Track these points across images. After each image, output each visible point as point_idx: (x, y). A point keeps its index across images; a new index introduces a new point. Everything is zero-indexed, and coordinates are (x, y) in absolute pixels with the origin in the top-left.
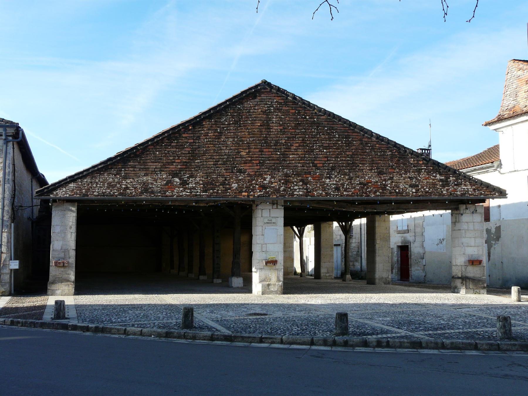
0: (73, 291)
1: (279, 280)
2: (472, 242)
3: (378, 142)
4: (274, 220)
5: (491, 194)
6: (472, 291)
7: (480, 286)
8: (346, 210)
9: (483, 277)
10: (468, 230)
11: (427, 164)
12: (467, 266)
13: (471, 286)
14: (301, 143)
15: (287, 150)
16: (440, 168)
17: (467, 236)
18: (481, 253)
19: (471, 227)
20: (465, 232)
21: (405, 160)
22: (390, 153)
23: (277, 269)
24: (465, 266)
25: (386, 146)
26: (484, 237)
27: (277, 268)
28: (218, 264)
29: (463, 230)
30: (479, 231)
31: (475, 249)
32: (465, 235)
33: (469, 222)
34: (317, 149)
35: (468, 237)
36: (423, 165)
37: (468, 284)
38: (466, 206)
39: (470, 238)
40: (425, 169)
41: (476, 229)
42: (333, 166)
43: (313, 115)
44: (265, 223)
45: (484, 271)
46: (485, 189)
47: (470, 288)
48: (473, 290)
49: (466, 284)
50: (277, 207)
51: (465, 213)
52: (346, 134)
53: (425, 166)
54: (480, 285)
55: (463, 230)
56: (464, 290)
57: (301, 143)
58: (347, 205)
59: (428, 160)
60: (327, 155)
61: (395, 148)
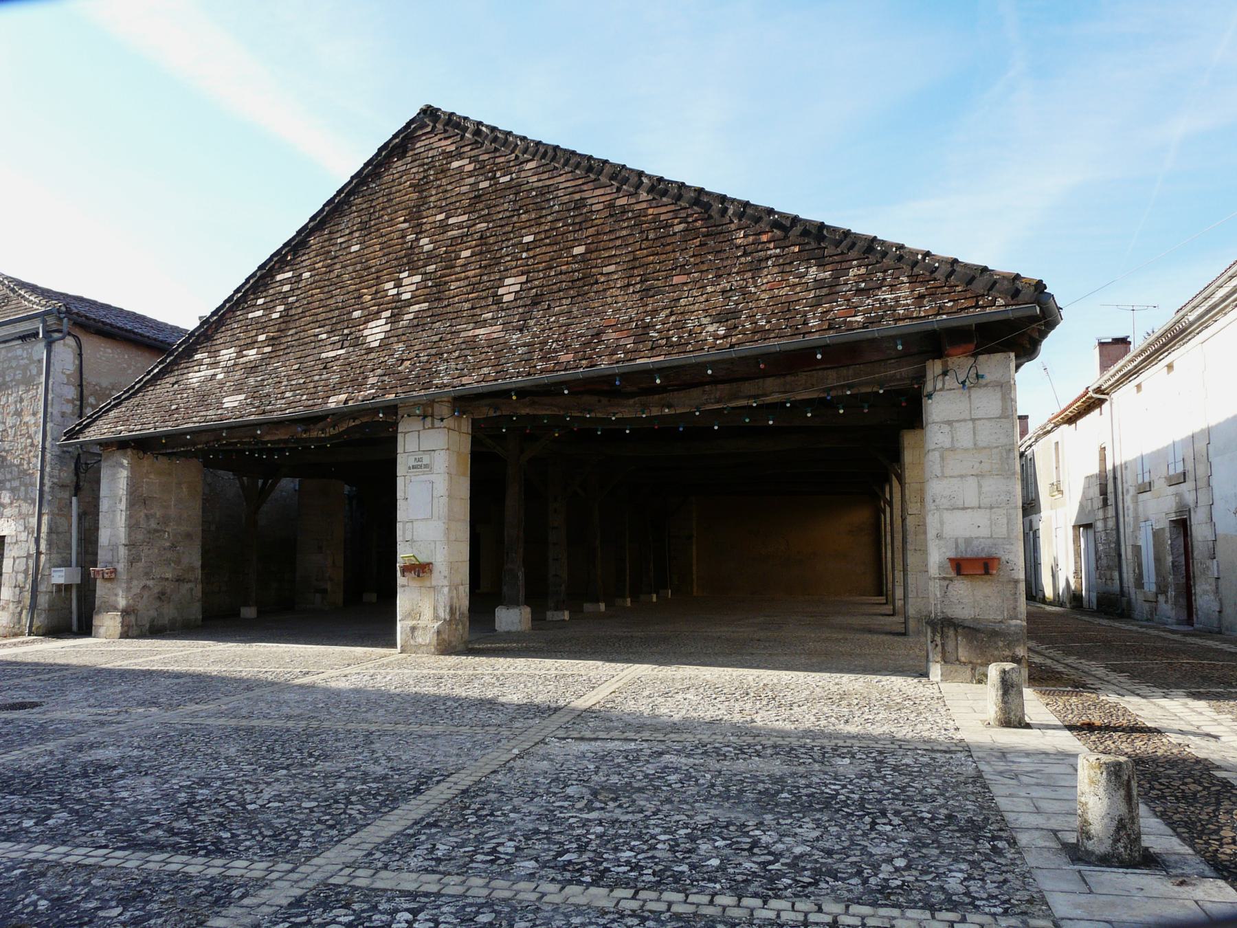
0: (119, 630)
1: (436, 618)
2: (968, 492)
3: (654, 199)
4: (426, 459)
5: (977, 306)
6: (969, 672)
7: (996, 653)
8: (593, 415)
9: (1014, 622)
10: (953, 449)
11: (786, 237)
12: (951, 580)
13: (963, 654)
14: (476, 246)
15: (448, 271)
16: (823, 245)
17: (948, 472)
18: (1002, 531)
19: (964, 436)
20: (942, 458)
21: (721, 240)
22: (682, 226)
23: (434, 587)
24: (944, 579)
25: (672, 207)
26: (1014, 474)
27: (434, 583)
28: (556, 575)
29: (933, 450)
30: (995, 451)
31: (982, 518)
32: (942, 467)
33: (957, 421)
34: (507, 255)
35: (951, 477)
36: (772, 245)
37: (950, 646)
38: (945, 365)
39: (962, 476)
40: (777, 256)
41: (984, 444)
42: (537, 295)
43: (512, 164)
44: (409, 468)
45: (1016, 600)
46: (959, 289)
47: (958, 660)
48: (970, 666)
49: (943, 645)
50: (433, 423)
51: (941, 390)
52: (577, 196)
53: (775, 248)
54: (997, 649)
55: (933, 450)
56: (938, 666)
57: (476, 246)
58: (599, 401)
59: (788, 224)
60: (528, 265)
61: (695, 208)
